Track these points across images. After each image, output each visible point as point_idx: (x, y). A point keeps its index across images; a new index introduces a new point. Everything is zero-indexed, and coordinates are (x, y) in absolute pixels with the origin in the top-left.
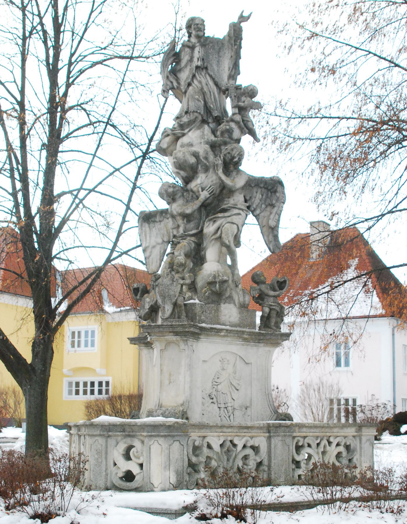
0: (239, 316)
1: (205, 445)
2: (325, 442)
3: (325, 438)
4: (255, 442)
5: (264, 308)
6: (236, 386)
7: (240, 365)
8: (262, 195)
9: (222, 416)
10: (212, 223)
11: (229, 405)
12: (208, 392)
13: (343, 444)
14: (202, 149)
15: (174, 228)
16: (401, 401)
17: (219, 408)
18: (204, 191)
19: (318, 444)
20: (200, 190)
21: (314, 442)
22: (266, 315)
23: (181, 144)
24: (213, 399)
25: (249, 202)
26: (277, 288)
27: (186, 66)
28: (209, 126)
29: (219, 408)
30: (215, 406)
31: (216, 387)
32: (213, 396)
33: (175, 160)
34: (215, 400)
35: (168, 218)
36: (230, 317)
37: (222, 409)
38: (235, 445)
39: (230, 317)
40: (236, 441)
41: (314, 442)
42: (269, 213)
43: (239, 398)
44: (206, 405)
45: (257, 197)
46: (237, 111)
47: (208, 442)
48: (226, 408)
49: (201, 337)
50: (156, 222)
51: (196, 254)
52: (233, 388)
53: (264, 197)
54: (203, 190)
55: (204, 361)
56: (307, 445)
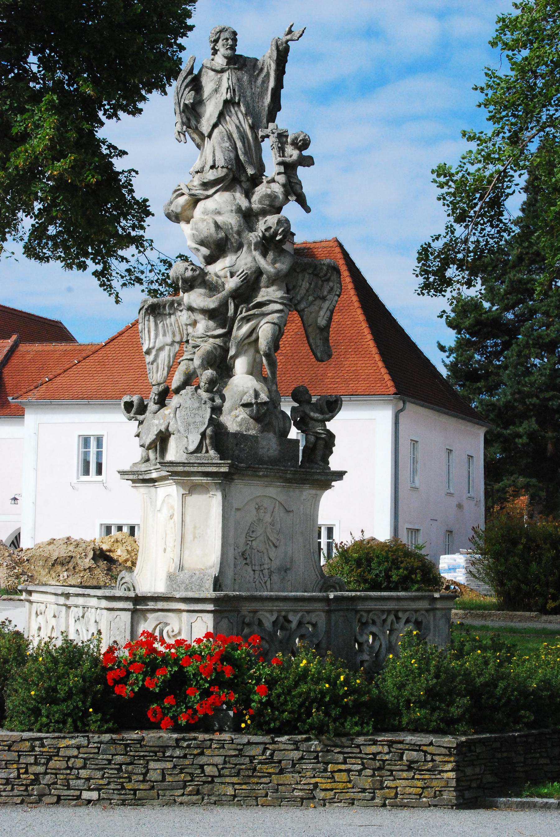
0: (279, 448)
1: (256, 622)
2: (392, 617)
3: (393, 612)
4: (313, 618)
5: (309, 437)
6: (275, 541)
7: (279, 512)
8: (310, 284)
9: (257, 581)
10: (245, 321)
11: (266, 566)
12: (241, 550)
13: (413, 620)
14: (231, 220)
15: (190, 325)
16: (405, 530)
17: (254, 571)
18: (235, 278)
19: (384, 621)
20: (228, 274)
21: (379, 617)
22: (311, 446)
23: (202, 210)
24: (246, 559)
25: (292, 292)
26: (326, 409)
27: (210, 97)
28: (241, 186)
29: (254, 571)
30: (249, 569)
31: (250, 543)
32: (247, 556)
33: (194, 232)
34: (248, 561)
35: (181, 311)
36: (269, 450)
37: (257, 573)
38: (289, 622)
39: (269, 450)
40: (291, 617)
41: (379, 617)
42: (317, 309)
43: (276, 557)
44: (239, 567)
45: (303, 286)
46: (282, 169)
47: (259, 619)
48: (262, 571)
49: (235, 477)
50: (165, 315)
51: (221, 363)
52: (271, 544)
53: (312, 286)
54: (232, 275)
55: (237, 509)
56: (371, 621)
